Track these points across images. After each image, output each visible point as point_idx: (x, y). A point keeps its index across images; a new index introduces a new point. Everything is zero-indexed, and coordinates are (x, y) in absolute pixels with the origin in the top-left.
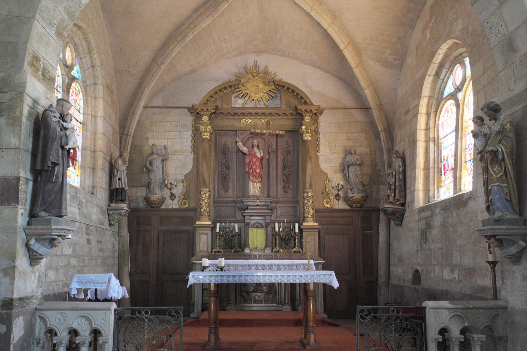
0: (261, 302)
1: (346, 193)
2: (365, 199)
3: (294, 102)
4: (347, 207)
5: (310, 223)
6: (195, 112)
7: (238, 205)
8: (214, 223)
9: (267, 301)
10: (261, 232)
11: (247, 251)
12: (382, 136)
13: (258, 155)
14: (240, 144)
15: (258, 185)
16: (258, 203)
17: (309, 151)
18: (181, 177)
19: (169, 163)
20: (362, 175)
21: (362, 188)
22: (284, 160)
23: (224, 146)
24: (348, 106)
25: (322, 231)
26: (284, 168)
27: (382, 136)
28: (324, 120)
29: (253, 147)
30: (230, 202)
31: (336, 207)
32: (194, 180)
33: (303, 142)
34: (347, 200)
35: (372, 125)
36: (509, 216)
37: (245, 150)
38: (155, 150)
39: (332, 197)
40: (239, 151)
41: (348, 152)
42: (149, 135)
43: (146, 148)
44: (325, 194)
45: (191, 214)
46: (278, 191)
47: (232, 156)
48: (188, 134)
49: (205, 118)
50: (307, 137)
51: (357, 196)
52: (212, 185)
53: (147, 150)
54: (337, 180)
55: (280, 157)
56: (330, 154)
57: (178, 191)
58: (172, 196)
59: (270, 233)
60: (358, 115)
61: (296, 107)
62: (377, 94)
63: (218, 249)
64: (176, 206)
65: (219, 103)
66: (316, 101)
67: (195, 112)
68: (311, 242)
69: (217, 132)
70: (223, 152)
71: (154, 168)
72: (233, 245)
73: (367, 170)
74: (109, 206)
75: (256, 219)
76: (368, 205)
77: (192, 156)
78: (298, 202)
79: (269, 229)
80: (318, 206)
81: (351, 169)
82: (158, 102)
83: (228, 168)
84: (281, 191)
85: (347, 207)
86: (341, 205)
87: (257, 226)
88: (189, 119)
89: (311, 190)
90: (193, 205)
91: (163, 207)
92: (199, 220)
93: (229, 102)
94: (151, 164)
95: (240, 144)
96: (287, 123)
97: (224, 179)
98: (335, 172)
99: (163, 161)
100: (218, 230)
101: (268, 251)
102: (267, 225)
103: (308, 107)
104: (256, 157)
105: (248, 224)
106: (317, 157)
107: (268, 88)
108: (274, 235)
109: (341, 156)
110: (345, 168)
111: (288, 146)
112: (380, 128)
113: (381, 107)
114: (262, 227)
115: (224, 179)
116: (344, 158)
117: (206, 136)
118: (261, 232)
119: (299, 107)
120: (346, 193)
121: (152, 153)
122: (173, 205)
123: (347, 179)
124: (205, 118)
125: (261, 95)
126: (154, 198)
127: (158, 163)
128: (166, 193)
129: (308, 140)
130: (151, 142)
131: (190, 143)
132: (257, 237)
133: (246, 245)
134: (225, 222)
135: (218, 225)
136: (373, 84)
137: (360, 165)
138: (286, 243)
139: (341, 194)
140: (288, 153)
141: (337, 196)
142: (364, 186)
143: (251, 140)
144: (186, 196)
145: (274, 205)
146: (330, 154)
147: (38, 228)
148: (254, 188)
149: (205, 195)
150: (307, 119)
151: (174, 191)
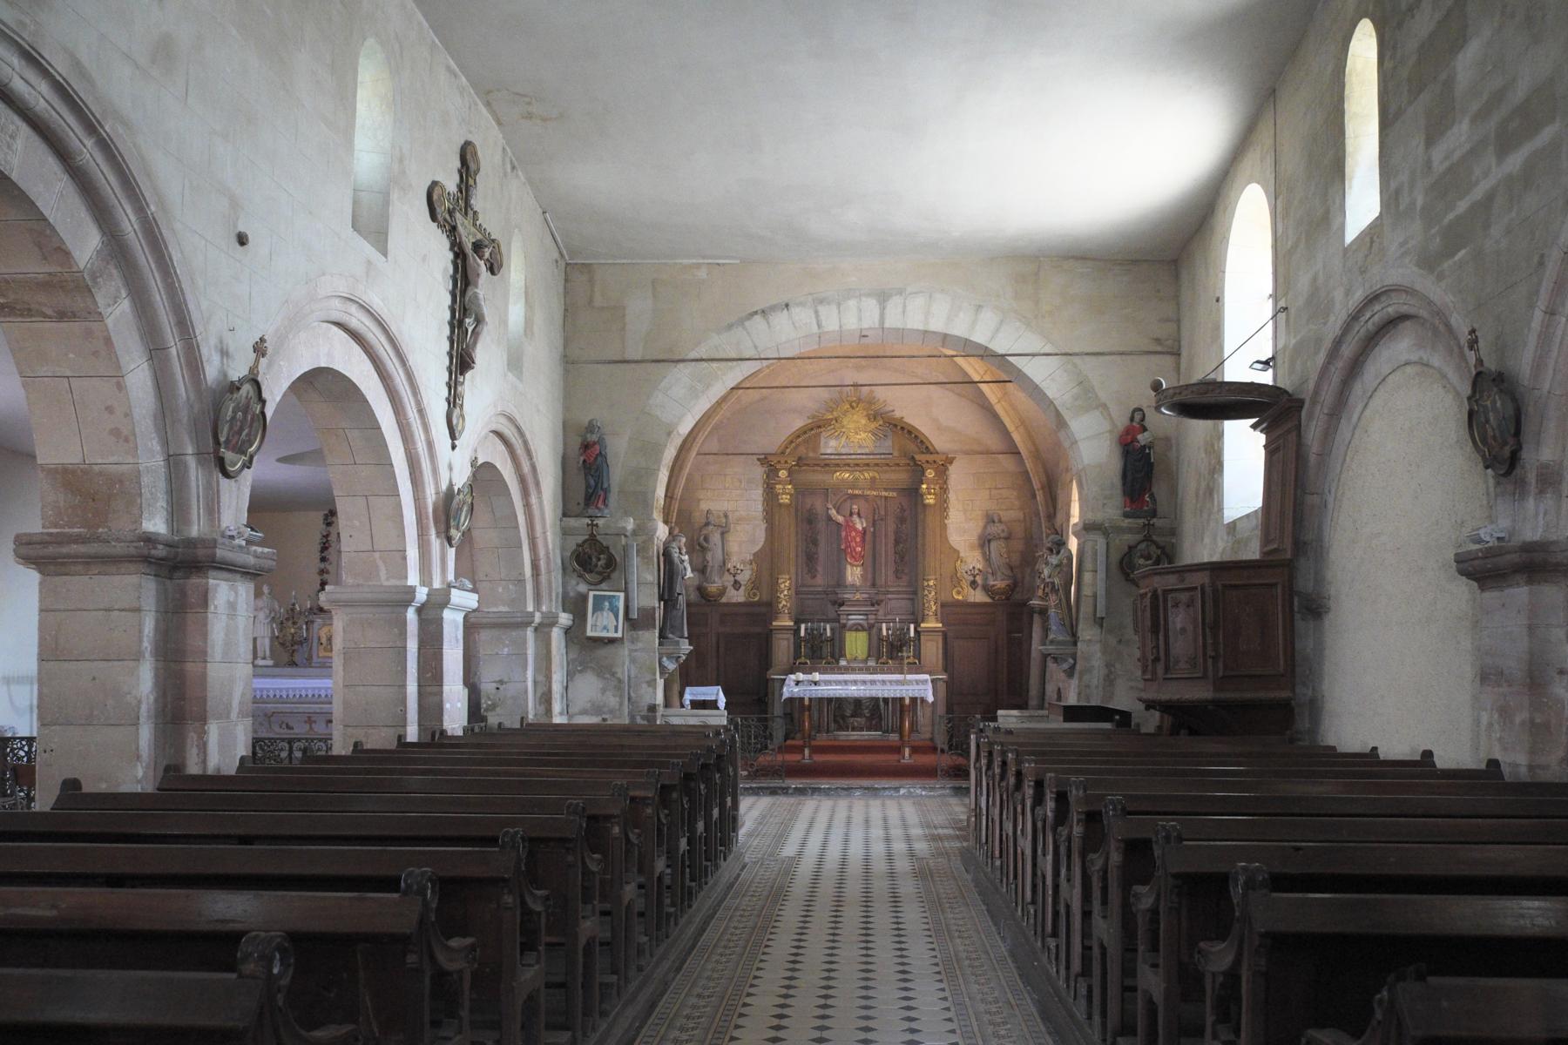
0: (861, 729)
1: (986, 579)
2: (1013, 587)
3: (912, 447)
4: (988, 600)
5: (931, 624)
6: (765, 460)
7: (832, 597)
8: (798, 622)
9: (869, 729)
10: (863, 636)
11: (843, 663)
12: (1040, 496)
13: (859, 527)
14: (833, 512)
15: (858, 571)
16: (858, 596)
17: (931, 520)
18: (749, 557)
19: (731, 537)
20: (1008, 552)
21: (1008, 572)
22: (897, 532)
23: (810, 511)
24: (994, 448)
25: (950, 634)
26: (897, 542)
27: (1040, 496)
28: (956, 473)
29: (851, 514)
30: (819, 593)
31: (971, 599)
32: (768, 560)
33: (925, 506)
34: (987, 589)
35: (1025, 474)
36: (1061, 638)
37: (840, 519)
38: (711, 519)
39: (965, 584)
40: (830, 518)
41: (990, 520)
42: (701, 494)
43: (697, 514)
44: (955, 580)
45: (763, 610)
46: (886, 573)
47: (821, 525)
48: (758, 494)
49: (783, 474)
50: (930, 500)
51: (1000, 584)
52: (793, 570)
53: (698, 518)
54: (973, 560)
55: (891, 527)
56: (963, 523)
57: (744, 577)
58: (737, 585)
59: (875, 639)
60: (1007, 463)
61: (914, 457)
62: (1030, 436)
63: (803, 660)
64: (741, 599)
65: (802, 451)
66: (939, 442)
67: (765, 460)
68: (932, 650)
69: (802, 491)
70: (808, 520)
71: (711, 545)
72: (821, 652)
73: (1018, 545)
74: (943, 751)
75: (855, 619)
76: (1017, 597)
77: (764, 526)
78: (915, 593)
79: (874, 631)
80: (944, 597)
81: (994, 545)
82: (714, 446)
83: (815, 543)
84: (891, 577)
85: (988, 600)
86: (978, 596)
87: (858, 628)
88: (759, 472)
89: (285, 982)
90: (765, 598)
91: (724, 600)
92: (776, 619)
93: (816, 448)
94: (706, 539)
95: (833, 512)
96: (901, 477)
97: (810, 559)
98: (972, 548)
99: (723, 534)
100: (802, 633)
101: (872, 663)
102: (871, 627)
103: (930, 458)
104: (856, 530)
105: (844, 626)
106: (944, 527)
107: (873, 425)
108: (880, 639)
109: (981, 524)
110: (985, 542)
111: (903, 510)
112: (1036, 484)
113: (1037, 455)
114: (864, 629)
115: (810, 559)
116: (985, 527)
117: (785, 499)
118: (863, 636)
119: (917, 457)
120: (986, 579)
121: (707, 524)
122: (738, 596)
123: (987, 559)
124: (783, 474)
125: (863, 435)
126: (712, 588)
127: (716, 538)
128: (729, 579)
129: (929, 505)
130: (704, 506)
131: (760, 507)
132: (856, 644)
133: (842, 655)
134: (812, 621)
135: (803, 627)
136: (1023, 423)
137: (1006, 539)
138: (893, 652)
139: (978, 579)
140: (902, 520)
141: (973, 584)
142: (1011, 569)
143: (848, 503)
144: (755, 584)
145: (881, 597)
146: (963, 523)
147: (669, 648)
148: (853, 574)
149: (785, 584)
150: (930, 474)
151: (738, 578)
